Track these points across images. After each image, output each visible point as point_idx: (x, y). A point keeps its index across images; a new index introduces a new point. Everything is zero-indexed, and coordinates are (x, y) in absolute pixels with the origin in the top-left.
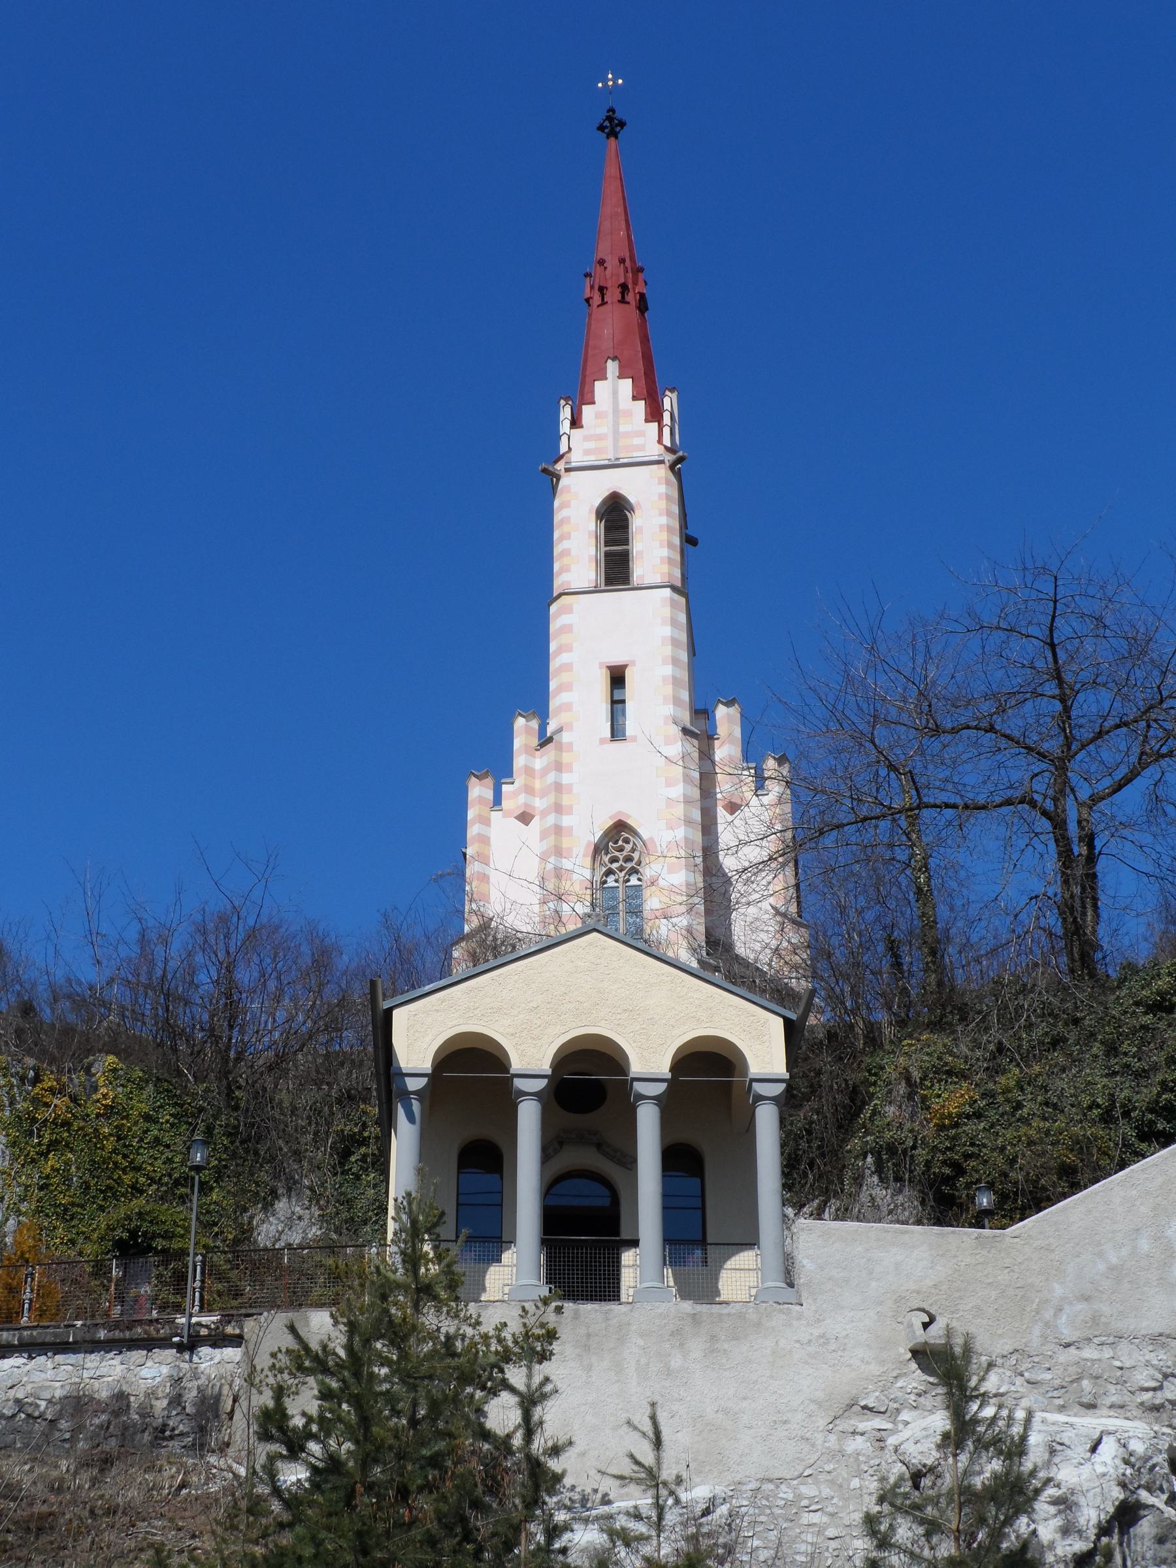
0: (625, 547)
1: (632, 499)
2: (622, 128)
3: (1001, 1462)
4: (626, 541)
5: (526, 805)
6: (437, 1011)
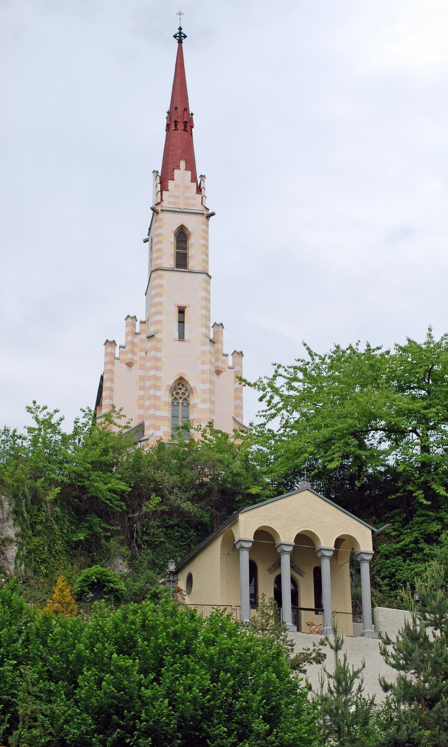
0: (185, 251)
1: (190, 229)
2: (176, 34)
3: (128, 571)
4: (186, 249)
5: (131, 359)
6: (254, 517)
